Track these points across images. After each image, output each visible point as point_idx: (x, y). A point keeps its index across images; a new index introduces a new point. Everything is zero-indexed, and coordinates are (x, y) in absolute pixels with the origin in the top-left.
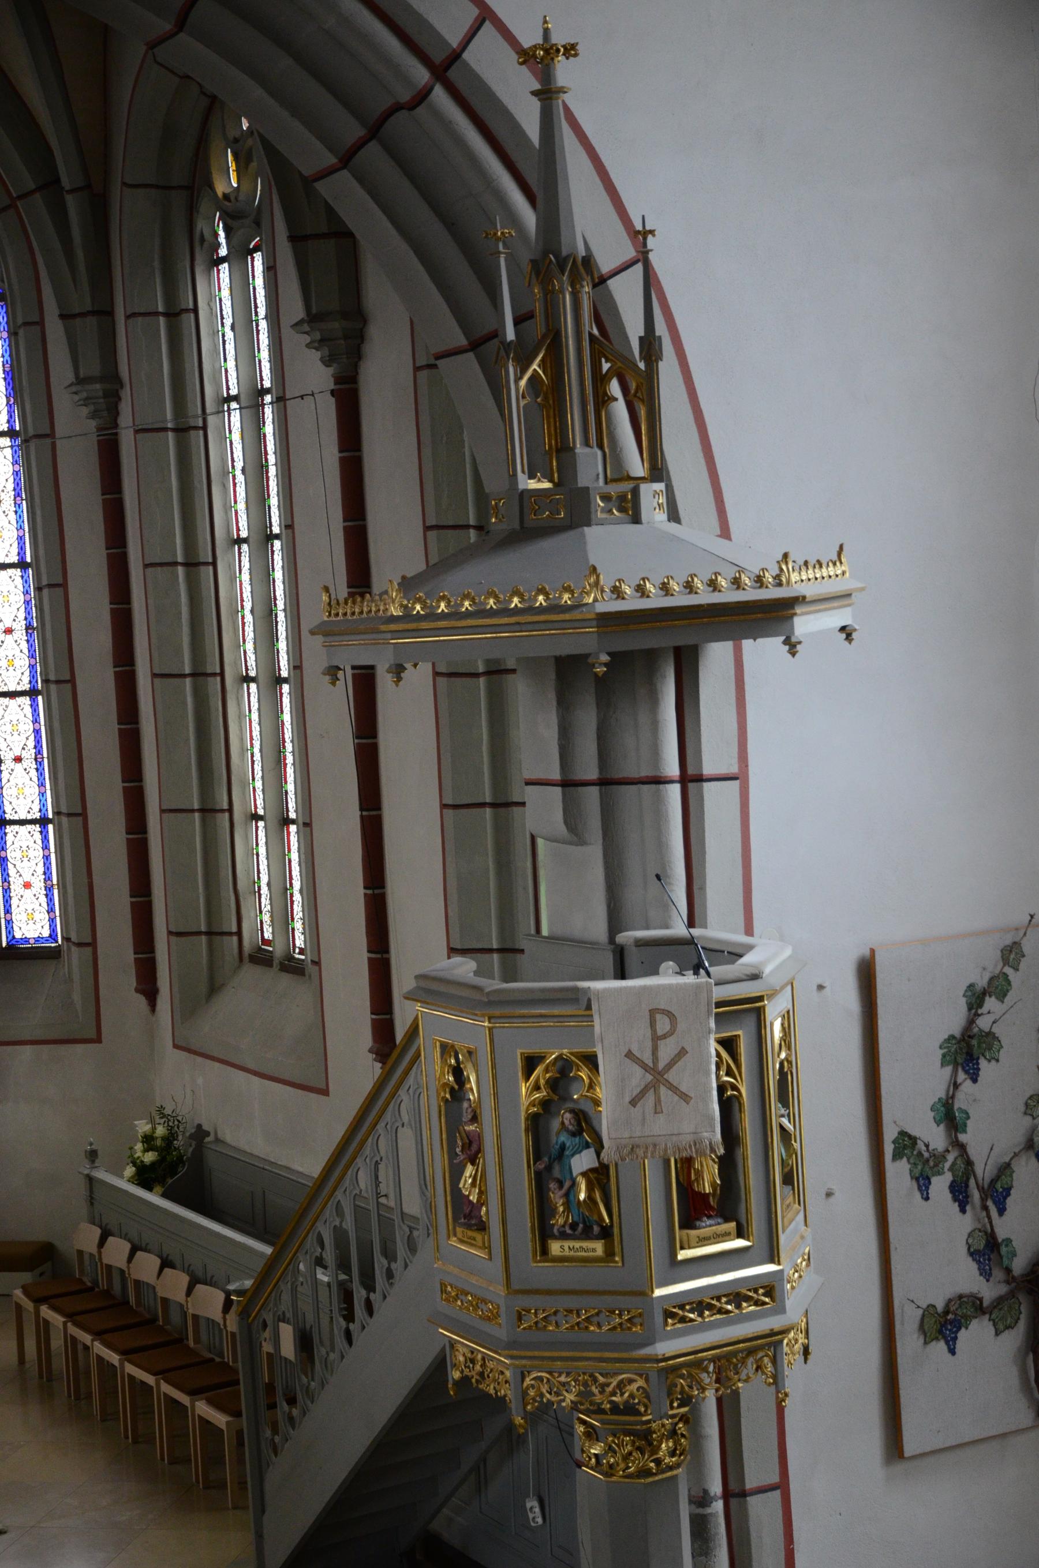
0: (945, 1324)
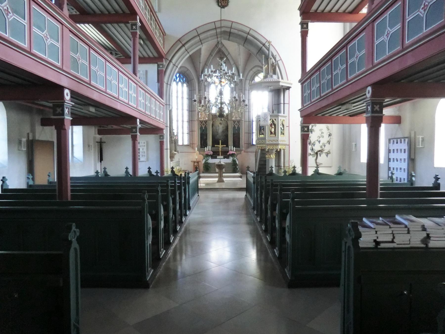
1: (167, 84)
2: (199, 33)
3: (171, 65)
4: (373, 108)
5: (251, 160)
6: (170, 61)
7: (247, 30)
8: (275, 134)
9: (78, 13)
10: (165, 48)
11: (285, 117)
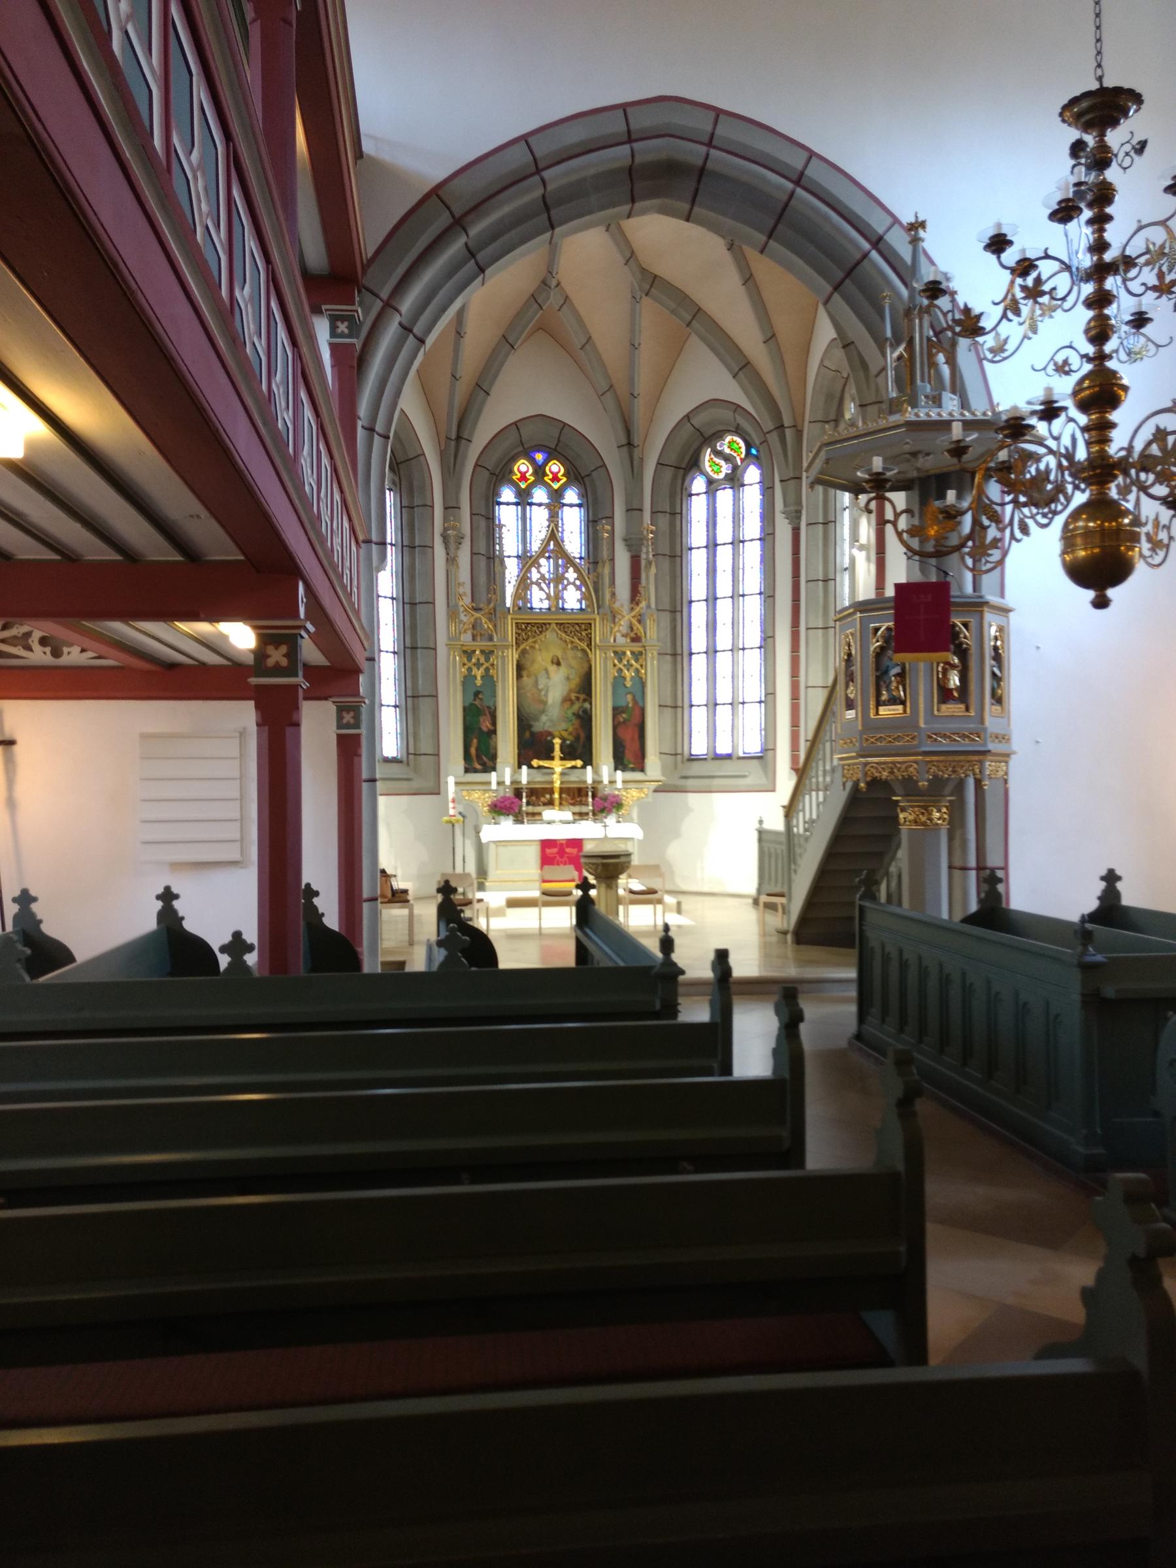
2: (457, 215)
6: (389, 306)
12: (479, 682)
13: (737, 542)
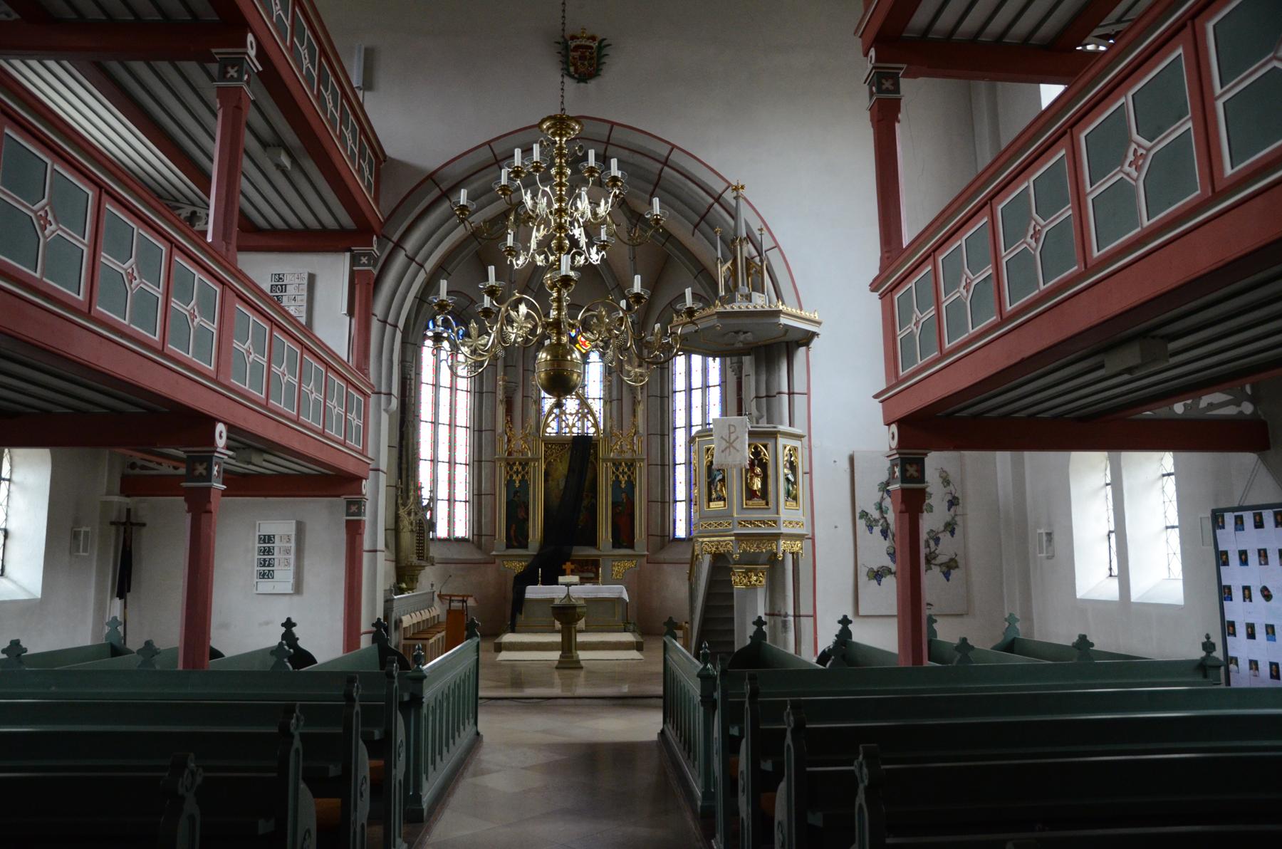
0: (877, 575)
1: (385, 322)
3: (400, 259)
4: (903, 471)
5: (679, 591)
6: (398, 245)
7: (663, 150)
8: (764, 493)
9: (15, 16)
10: (381, 202)
11: (799, 437)
12: (517, 484)
13: (705, 387)
